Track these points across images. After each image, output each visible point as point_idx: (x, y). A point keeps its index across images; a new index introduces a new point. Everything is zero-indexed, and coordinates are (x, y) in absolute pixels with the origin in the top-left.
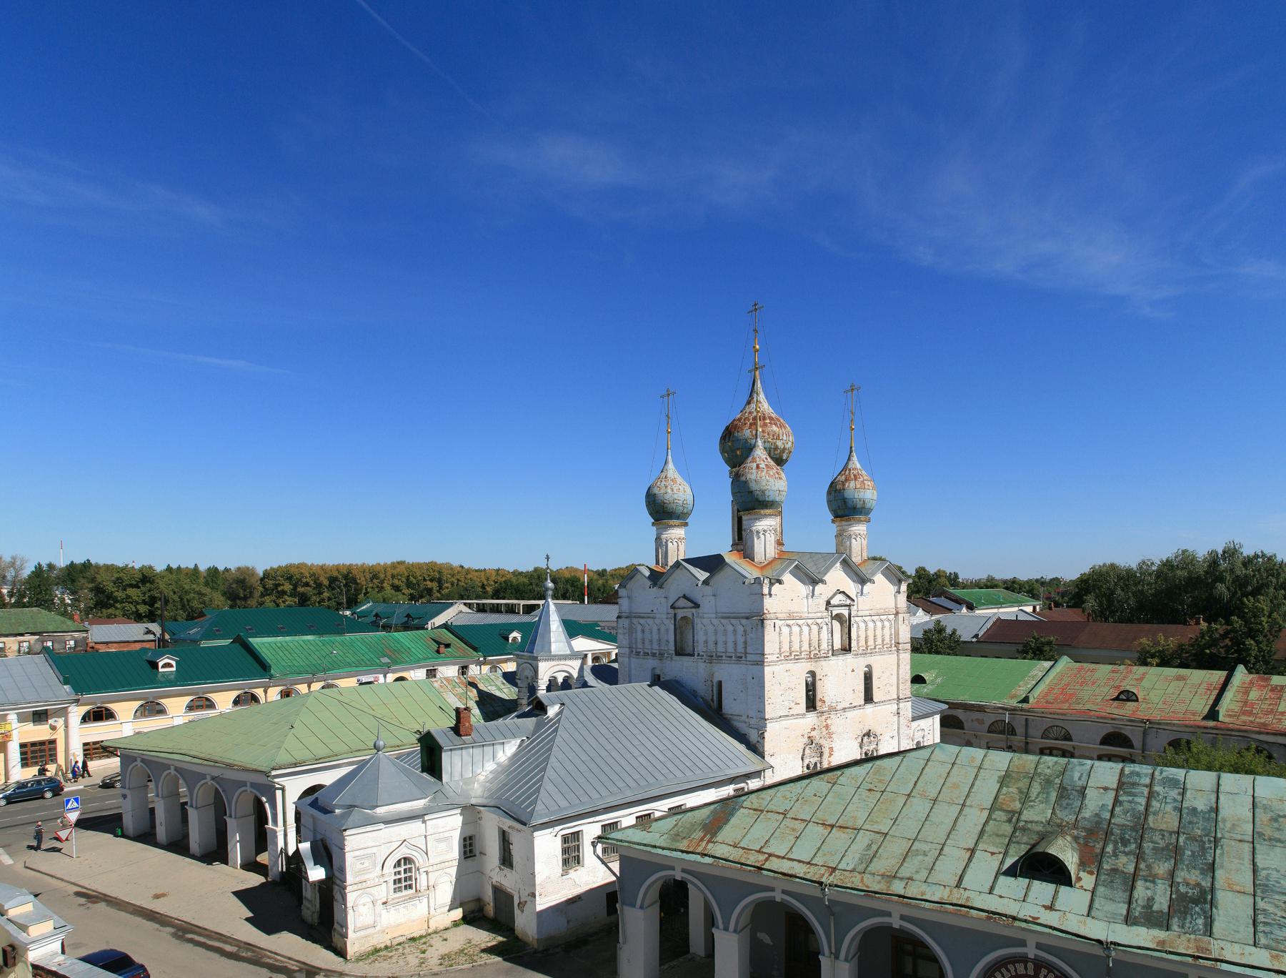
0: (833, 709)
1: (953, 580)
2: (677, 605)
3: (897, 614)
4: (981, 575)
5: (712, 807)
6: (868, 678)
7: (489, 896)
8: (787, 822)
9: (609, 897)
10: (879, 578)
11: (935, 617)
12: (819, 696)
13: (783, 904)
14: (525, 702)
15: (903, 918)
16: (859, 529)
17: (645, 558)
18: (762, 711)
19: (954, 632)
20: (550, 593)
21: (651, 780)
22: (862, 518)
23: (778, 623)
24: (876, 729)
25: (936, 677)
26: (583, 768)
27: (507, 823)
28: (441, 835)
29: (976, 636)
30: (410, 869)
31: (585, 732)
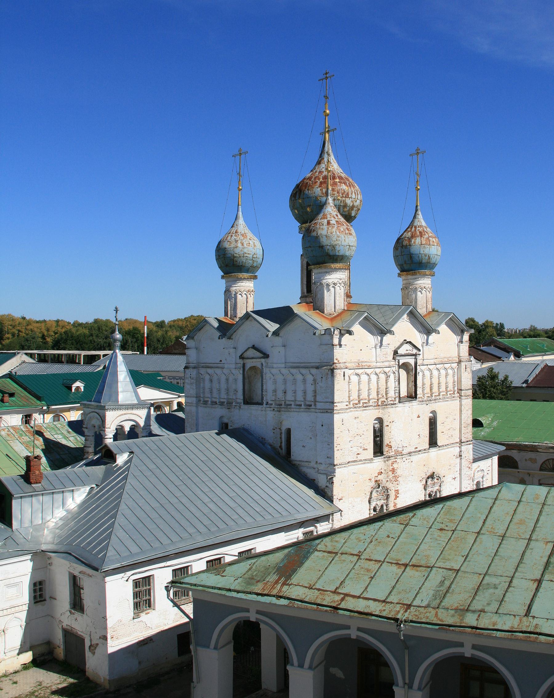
0: (399, 454)
1: (500, 330)
3: (460, 362)
4: (523, 325)
5: (286, 551)
6: (433, 423)
7: (59, 639)
8: (362, 563)
9: (181, 639)
10: (443, 328)
11: (487, 365)
12: (386, 441)
13: (358, 641)
14: (91, 450)
15: (474, 647)
16: (424, 282)
17: (214, 312)
18: (331, 457)
19: (506, 378)
20: (118, 344)
21: (222, 526)
22: (427, 272)
23: (348, 372)
24: (440, 471)
25: (492, 421)
26: (154, 515)
27: (78, 569)
28: (12, 581)
29: (526, 382)
31: (154, 480)
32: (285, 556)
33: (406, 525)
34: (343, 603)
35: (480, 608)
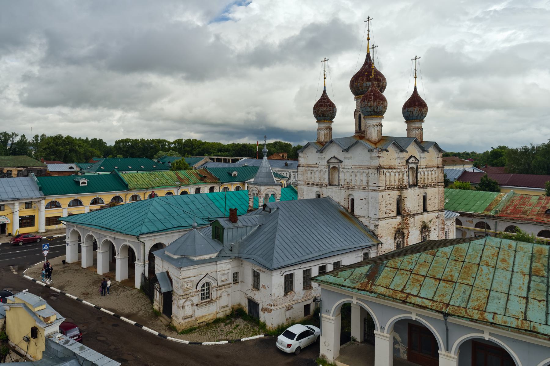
2: (330, 161)
6: (425, 198)
28: (224, 272)
30: (209, 288)
32: (370, 268)
33: (435, 256)
34: (408, 299)
35: (493, 311)
